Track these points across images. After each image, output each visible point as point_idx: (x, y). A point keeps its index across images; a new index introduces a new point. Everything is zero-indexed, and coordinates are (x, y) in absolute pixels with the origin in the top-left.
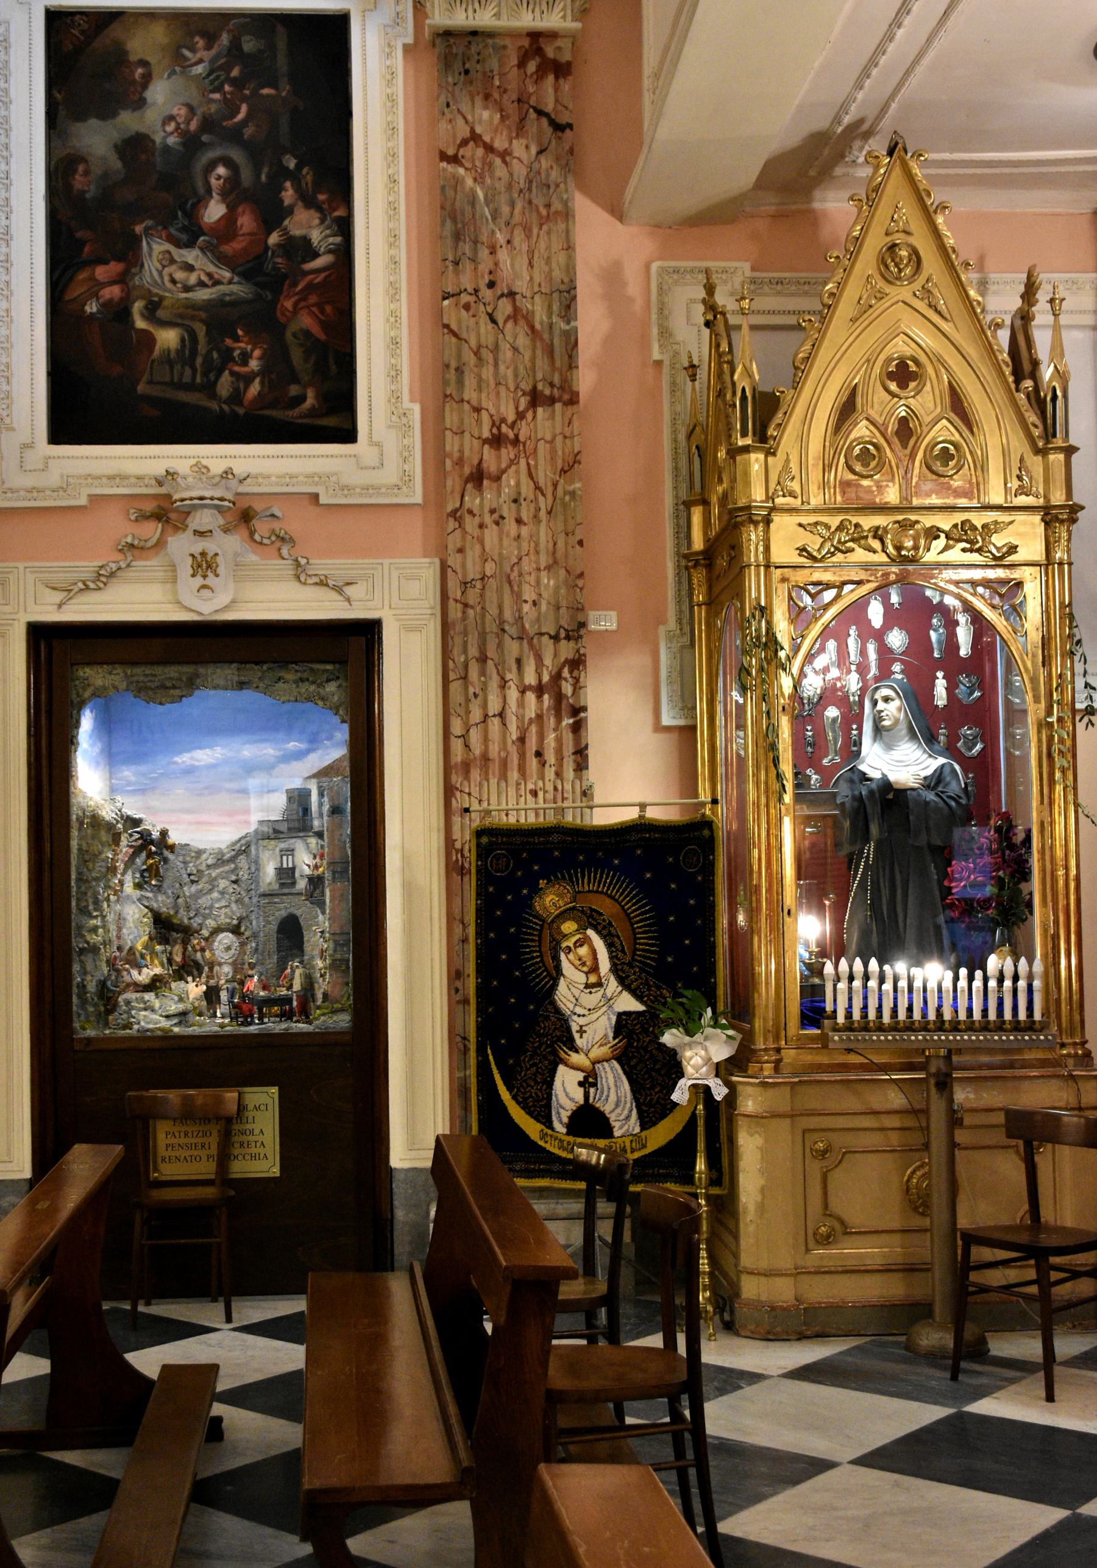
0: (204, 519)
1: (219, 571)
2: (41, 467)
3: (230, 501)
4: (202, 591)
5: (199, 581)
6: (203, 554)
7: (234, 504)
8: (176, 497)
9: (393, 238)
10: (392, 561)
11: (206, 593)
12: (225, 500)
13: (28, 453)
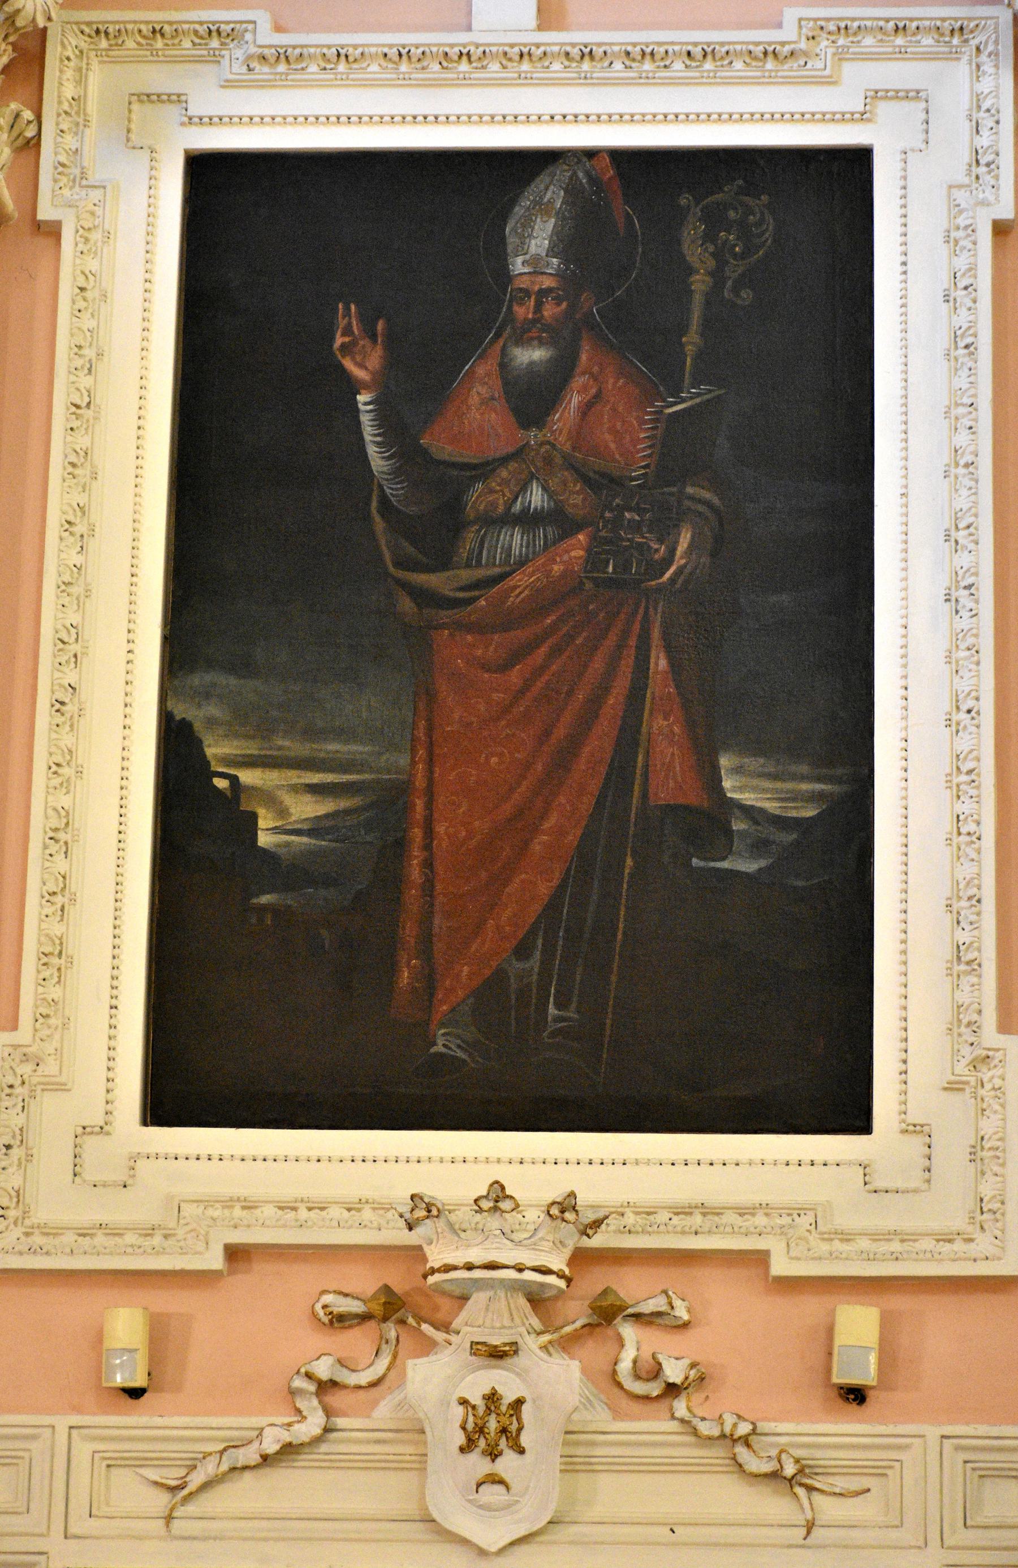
0: (485, 1318)
1: (525, 1440)
2: (121, 1176)
3: (561, 1275)
4: (481, 1489)
5: (477, 1464)
6: (492, 1398)
7: (569, 1281)
8: (436, 1257)
9: (76, 585)
10: (75, 1420)
11: (492, 1494)
12: (455, 1268)
13: (90, 1143)
